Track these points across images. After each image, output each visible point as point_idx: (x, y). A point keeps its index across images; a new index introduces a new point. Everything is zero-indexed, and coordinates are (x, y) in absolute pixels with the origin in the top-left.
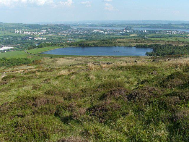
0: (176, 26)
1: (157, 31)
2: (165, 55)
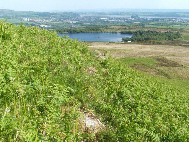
0: (182, 15)
1: (161, 19)
2: (139, 40)
